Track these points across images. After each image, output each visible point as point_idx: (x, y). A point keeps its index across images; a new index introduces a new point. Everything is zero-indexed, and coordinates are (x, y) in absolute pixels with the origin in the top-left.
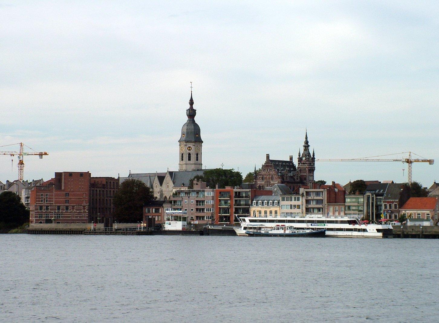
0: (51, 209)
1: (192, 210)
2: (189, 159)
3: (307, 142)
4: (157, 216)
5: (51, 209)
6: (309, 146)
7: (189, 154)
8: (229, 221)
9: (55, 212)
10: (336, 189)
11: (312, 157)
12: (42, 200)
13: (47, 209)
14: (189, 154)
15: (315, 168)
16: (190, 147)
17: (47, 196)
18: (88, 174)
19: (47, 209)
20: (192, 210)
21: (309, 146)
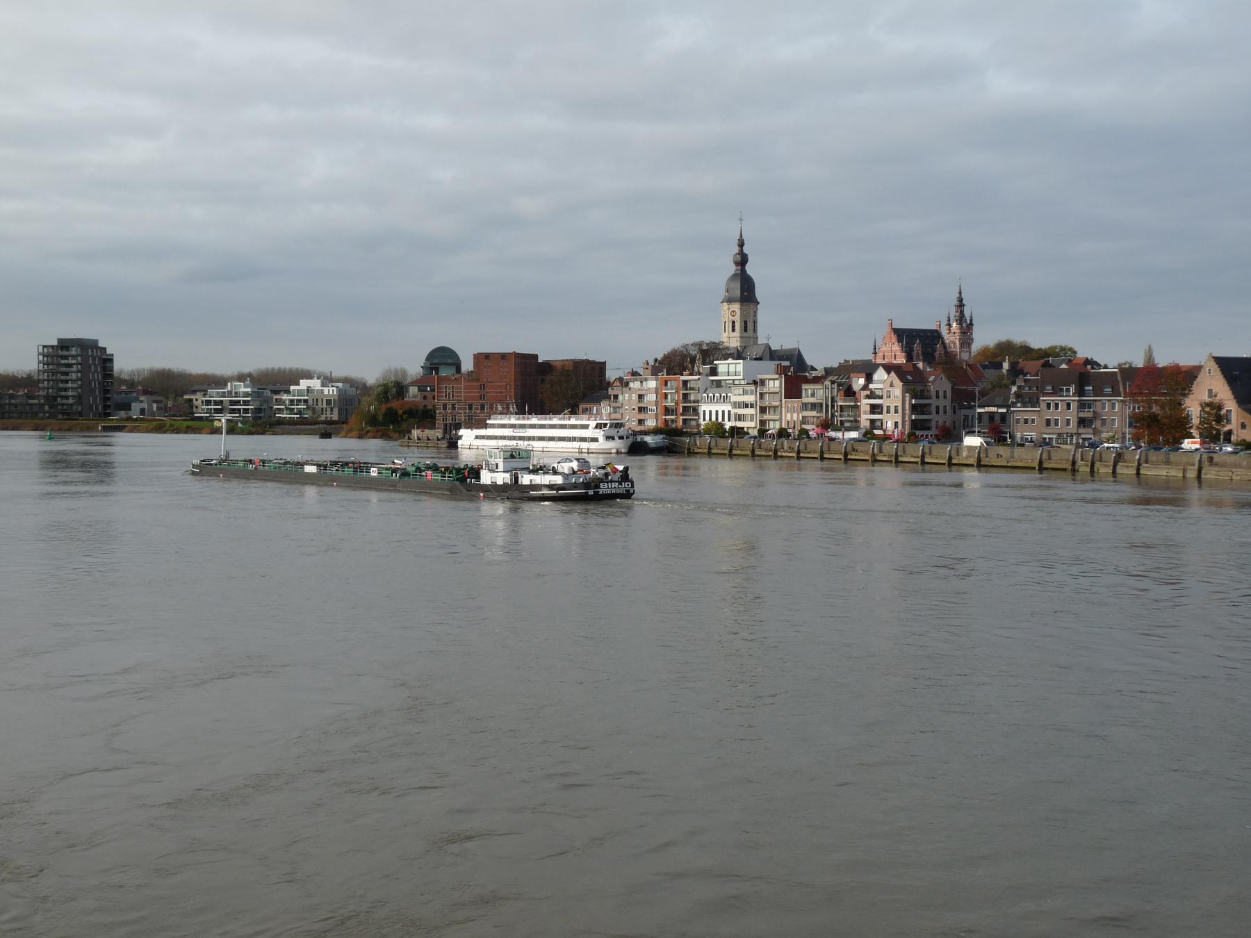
0: (459, 409)
1: (634, 409)
2: (733, 330)
3: (961, 300)
4: (778, 417)
5: (459, 409)
6: (964, 305)
7: (733, 322)
8: (101, 431)
9: (465, 413)
10: (169, 406)
11: (968, 322)
12: (446, 396)
13: (454, 408)
14: (733, 322)
15: (972, 339)
16: (734, 311)
17: (453, 389)
18: (535, 357)
19: (454, 408)
20: (634, 409)
21: (964, 305)
